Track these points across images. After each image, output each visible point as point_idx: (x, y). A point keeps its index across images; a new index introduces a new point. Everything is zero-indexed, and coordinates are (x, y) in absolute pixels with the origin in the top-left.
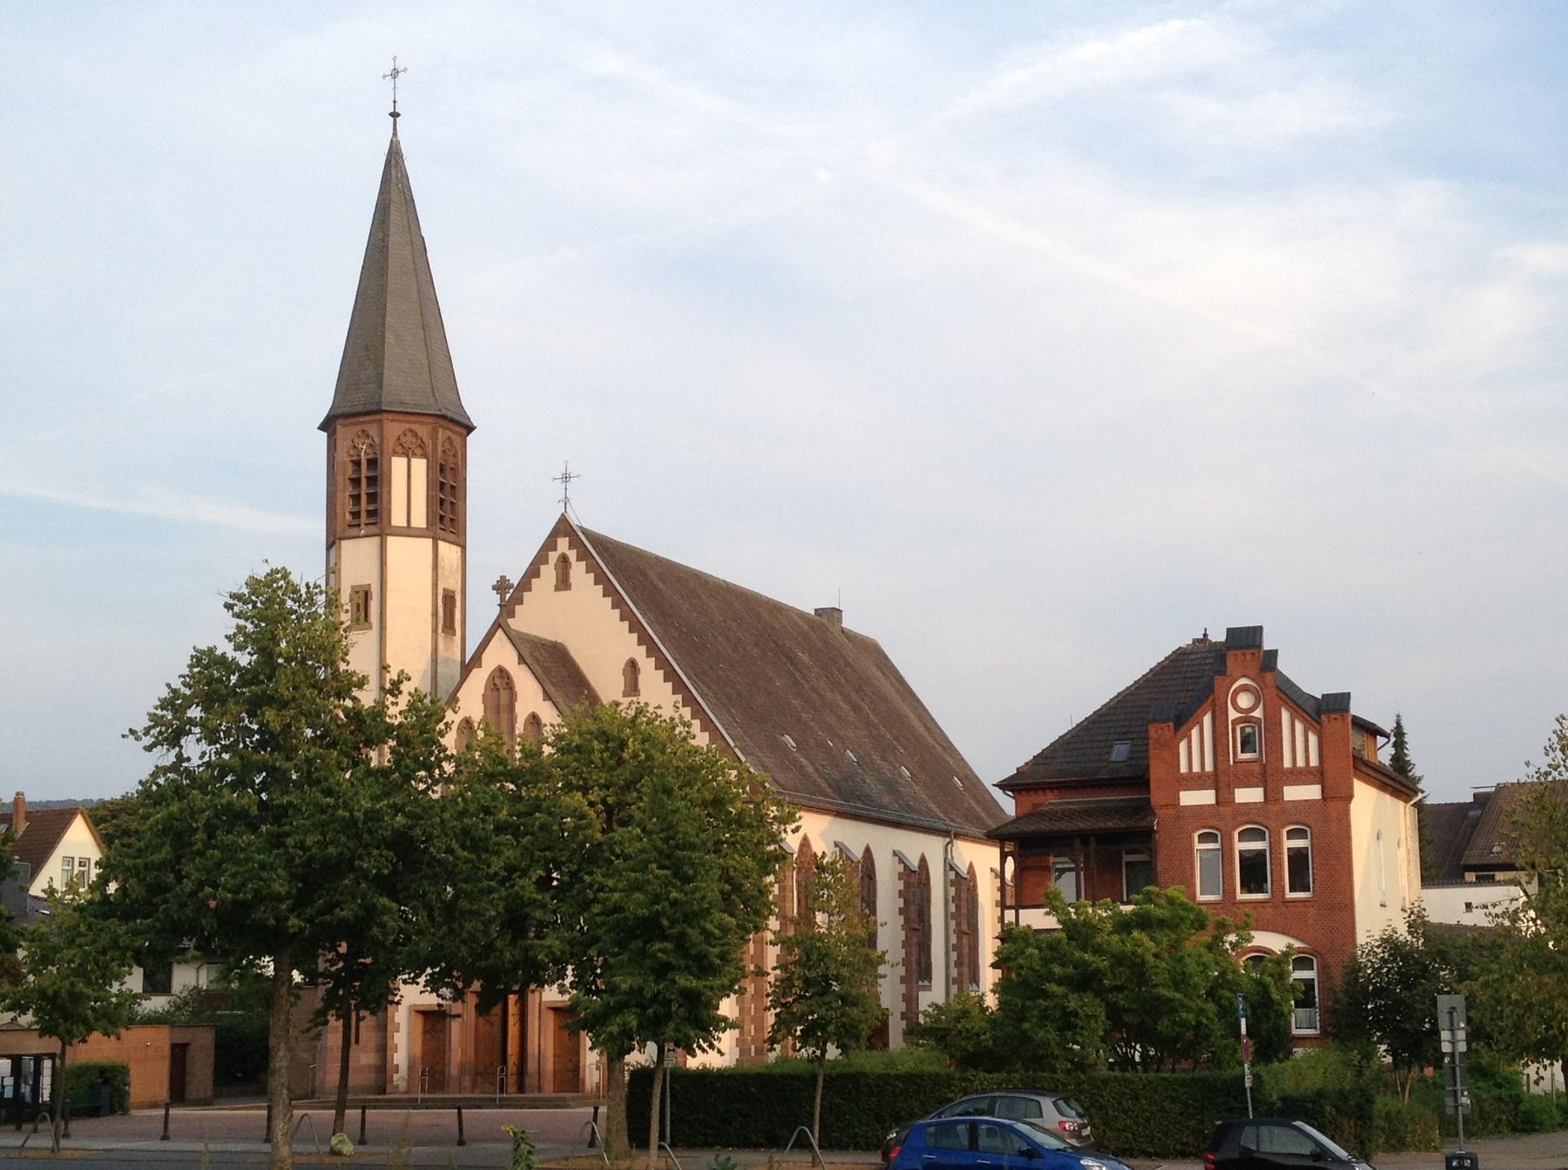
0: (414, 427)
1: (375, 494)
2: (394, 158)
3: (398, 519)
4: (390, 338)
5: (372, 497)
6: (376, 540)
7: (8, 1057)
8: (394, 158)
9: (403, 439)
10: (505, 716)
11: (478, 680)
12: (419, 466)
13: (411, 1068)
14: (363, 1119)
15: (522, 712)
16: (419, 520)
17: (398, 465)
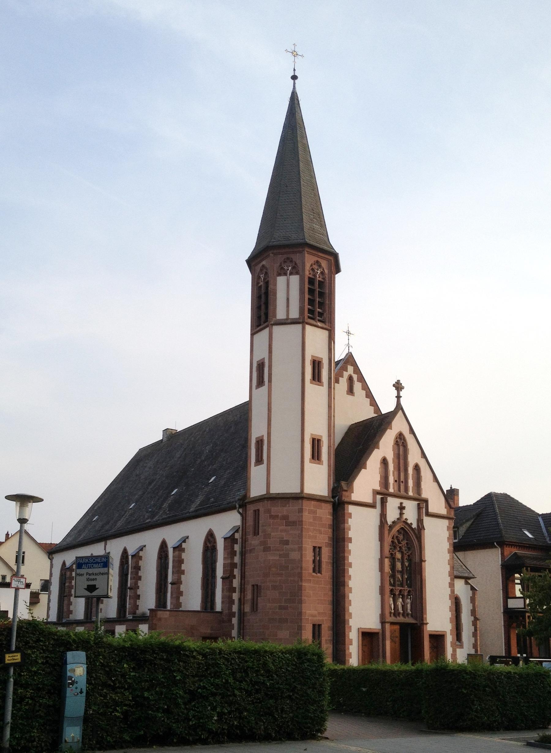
2: (294, 100)
3: (281, 314)
8: (294, 100)
12: (295, 280)
16: (294, 314)
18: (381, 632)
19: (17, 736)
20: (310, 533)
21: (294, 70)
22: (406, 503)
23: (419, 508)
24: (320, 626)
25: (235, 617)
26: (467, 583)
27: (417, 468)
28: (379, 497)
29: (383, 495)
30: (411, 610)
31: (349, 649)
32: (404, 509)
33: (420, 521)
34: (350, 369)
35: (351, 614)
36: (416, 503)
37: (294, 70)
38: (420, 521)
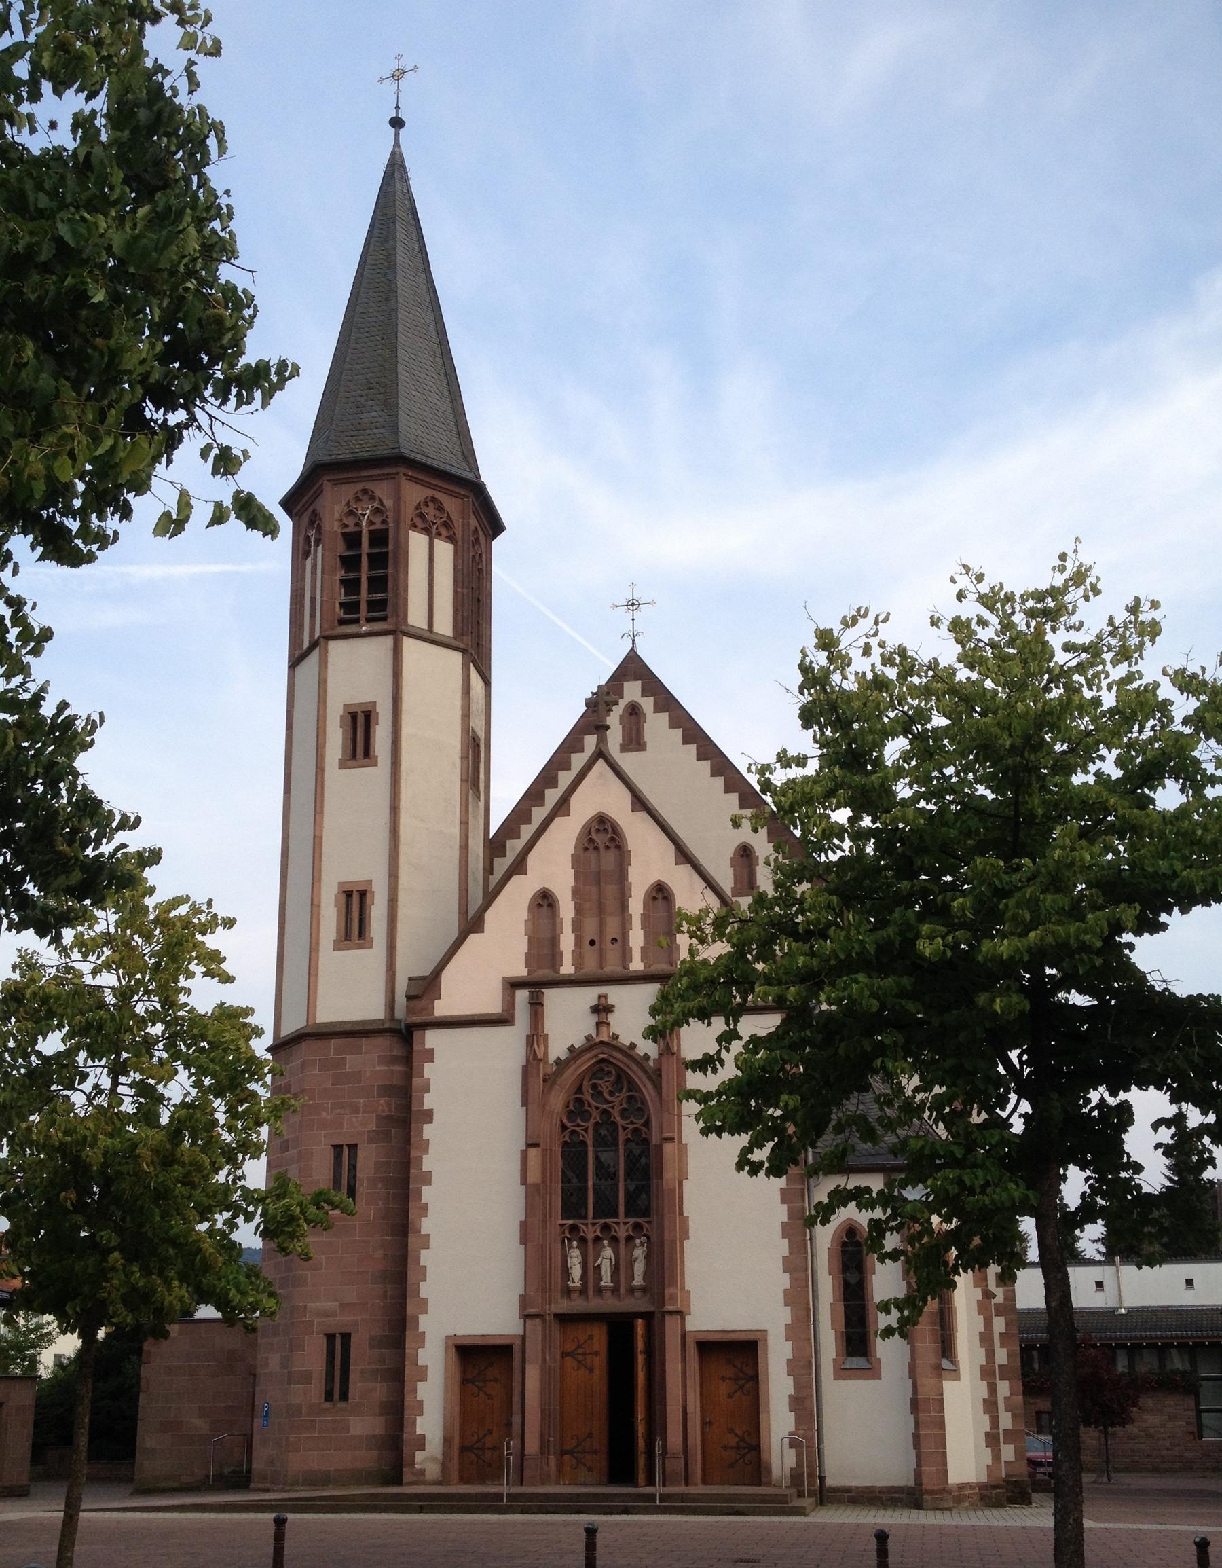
0: (439, 495)
1: (384, 578)
2: (396, 170)
3: (416, 617)
4: (403, 375)
5: (378, 583)
6: (388, 640)
7: (514, 994)
8: (396, 170)
9: (424, 510)
10: (610, 890)
11: (563, 838)
13: (447, 1441)
14: (279, 1536)
15: (640, 880)
17: (417, 542)
18: (518, 1342)
20: (324, 1114)
21: (397, 107)
22: (616, 995)
24: (346, 1337)
25: (1001, 1334)
28: (522, 996)
29: (535, 984)
30: (646, 1276)
31: (415, 1391)
34: (632, 690)
35: (425, 1301)
37: (397, 107)
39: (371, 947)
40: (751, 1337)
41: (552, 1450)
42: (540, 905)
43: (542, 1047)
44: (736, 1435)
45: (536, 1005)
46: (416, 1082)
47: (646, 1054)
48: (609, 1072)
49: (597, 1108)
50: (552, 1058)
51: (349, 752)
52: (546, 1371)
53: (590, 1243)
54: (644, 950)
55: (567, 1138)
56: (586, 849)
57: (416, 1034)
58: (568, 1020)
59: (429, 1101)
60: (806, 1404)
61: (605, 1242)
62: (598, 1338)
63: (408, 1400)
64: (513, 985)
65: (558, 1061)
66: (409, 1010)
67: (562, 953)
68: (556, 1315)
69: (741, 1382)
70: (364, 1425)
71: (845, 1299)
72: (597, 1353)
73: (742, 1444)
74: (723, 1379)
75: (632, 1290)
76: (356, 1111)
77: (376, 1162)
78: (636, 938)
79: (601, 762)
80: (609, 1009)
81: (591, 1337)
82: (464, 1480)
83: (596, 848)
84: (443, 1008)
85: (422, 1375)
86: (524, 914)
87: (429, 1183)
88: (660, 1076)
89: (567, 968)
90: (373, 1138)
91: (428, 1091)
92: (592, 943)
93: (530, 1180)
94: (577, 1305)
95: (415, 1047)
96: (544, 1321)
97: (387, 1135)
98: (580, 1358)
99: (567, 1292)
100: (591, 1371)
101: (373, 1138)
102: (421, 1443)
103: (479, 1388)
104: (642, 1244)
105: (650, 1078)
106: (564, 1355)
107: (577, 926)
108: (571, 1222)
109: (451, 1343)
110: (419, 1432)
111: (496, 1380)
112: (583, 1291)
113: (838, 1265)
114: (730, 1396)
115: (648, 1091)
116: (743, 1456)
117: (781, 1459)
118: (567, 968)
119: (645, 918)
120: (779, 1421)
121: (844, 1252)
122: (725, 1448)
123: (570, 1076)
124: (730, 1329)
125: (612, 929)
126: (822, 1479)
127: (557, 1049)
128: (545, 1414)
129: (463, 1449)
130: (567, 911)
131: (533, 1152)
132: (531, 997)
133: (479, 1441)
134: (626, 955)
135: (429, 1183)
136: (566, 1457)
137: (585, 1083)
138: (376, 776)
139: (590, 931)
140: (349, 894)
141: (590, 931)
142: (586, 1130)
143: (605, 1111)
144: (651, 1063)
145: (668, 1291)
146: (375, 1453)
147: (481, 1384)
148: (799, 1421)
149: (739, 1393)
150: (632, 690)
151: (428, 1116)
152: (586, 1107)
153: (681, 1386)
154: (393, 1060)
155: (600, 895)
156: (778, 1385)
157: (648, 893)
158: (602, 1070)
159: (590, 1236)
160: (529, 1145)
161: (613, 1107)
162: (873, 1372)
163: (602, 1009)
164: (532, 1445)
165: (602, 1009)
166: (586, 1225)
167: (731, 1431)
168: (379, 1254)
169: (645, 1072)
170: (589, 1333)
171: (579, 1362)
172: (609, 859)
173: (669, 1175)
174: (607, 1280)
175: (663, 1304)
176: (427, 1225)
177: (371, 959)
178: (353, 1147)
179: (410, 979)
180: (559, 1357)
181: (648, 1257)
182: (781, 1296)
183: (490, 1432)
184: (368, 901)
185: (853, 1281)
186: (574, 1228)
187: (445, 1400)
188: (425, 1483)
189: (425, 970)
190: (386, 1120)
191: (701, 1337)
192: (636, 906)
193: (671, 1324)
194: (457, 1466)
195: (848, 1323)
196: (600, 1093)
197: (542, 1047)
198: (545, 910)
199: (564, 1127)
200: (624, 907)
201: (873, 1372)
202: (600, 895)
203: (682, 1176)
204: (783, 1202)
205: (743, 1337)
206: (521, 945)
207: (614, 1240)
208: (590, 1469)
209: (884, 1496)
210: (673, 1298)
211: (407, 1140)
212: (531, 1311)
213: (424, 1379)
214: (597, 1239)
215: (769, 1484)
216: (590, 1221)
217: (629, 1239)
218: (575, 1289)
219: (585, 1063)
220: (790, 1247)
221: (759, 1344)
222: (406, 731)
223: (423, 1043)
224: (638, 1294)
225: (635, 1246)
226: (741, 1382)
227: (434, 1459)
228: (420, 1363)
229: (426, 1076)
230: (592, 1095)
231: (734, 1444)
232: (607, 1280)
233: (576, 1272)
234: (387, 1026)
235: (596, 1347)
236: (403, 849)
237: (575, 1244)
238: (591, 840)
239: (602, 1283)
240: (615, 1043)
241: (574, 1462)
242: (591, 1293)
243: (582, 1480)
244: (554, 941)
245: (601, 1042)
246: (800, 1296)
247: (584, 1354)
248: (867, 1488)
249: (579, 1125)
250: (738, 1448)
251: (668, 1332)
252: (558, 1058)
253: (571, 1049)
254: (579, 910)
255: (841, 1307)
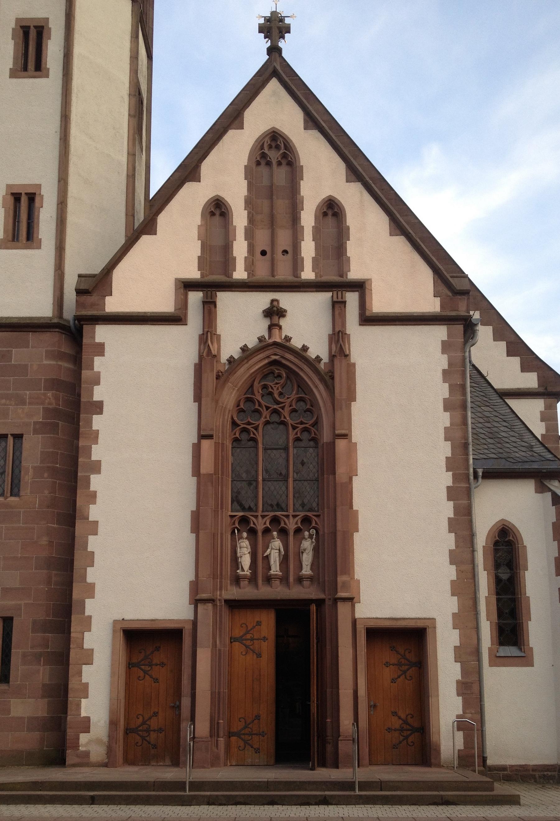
10: (282, 205)
13: (113, 724)
18: (188, 628)
19: (250, 760)
22: (286, 300)
23: (338, 306)
26: (541, 488)
27: (331, 209)
28: (195, 298)
29: (210, 285)
31: (80, 673)
32: (284, 316)
33: (338, 339)
35: (92, 587)
36: (325, 297)
38: (338, 339)
39: (39, 247)
40: (420, 624)
41: (221, 734)
42: (212, 214)
43: (216, 345)
44: (400, 718)
45: (209, 305)
46: (85, 374)
47: (318, 357)
48: (279, 376)
49: (268, 408)
50: (224, 357)
51: (21, 62)
52: (216, 656)
53: (260, 534)
54: (315, 261)
55: (237, 435)
56: (258, 163)
57: (86, 328)
58: (240, 322)
59: (97, 453)
60: (471, 690)
61: (275, 533)
62: (267, 623)
63: (73, 684)
64: (187, 286)
65: (231, 360)
66: (79, 304)
67: (235, 259)
68: (226, 601)
69: (404, 668)
70: (26, 706)
71: (498, 594)
72: (265, 639)
73: (405, 727)
74: (387, 664)
75: (300, 580)
76: (22, 402)
77: (42, 453)
78: (308, 249)
79: (274, 84)
80: (281, 313)
81: (259, 623)
82: (129, 761)
83: (269, 164)
84: (113, 304)
85: (88, 657)
86: (197, 220)
87: (101, 412)
88: (332, 378)
89: (240, 273)
90: (39, 429)
91: (98, 383)
92: (264, 253)
93: (203, 471)
94: (246, 592)
95: (85, 341)
96: (215, 606)
97: (54, 428)
98: (248, 643)
99: (237, 580)
100: (259, 656)
101: (39, 429)
102: (85, 725)
103: (145, 672)
104: (311, 536)
105: (322, 379)
106: (233, 640)
107: (249, 235)
108: (241, 514)
109: (119, 627)
110: (83, 714)
111: (162, 664)
112: (253, 579)
113: (491, 563)
114: (393, 681)
115: (320, 393)
116: (406, 738)
117: (448, 740)
118: (240, 273)
119: (317, 231)
120: (447, 706)
121: (496, 551)
122: (389, 730)
123: (243, 374)
124: (406, 617)
125: (283, 239)
126: (484, 759)
127: (229, 348)
128: (216, 698)
129: (128, 731)
130: (240, 219)
131: (206, 444)
132: (205, 296)
133: (144, 723)
134: (297, 264)
135: (101, 412)
136: (233, 739)
137: (256, 383)
138: (48, 86)
139: (262, 242)
140: (17, 197)
141: (262, 242)
142: (256, 428)
143: (275, 411)
144: (322, 366)
145: (341, 579)
146: (37, 735)
147: (147, 668)
148: (466, 705)
149: (402, 678)
150: (274, 111)
151: (96, 467)
152: (270, 390)
153: (351, 671)
154: (61, 356)
155: (272, 207)
156: (446, 671)
157: (319, 208)
158: (273, 373)
159: (260, 527)
160: (202, 437)
161: (283, 408)
162: (525, 659)
163: (274, 313)
164: (202, 727)
165: (274, 313)
166: (256, 517)
167: (395, 714)
168: (44, 541)
169: (316, 371)
170: (257, 619)
171: (247, 647)
172: (281, 175)
173: (341, 470)
174: (275, 569)
175: (336, 592)
176: (95, 512)
177: (42, 258)
178: (18, 437)
179: (80, 276)
180: (227, 641)
181: (316, 550)
182: (448, 587)
183: (156, 714)
184: (37, 204)
185: (504, 577)
186: (244, 520)
187: (112, 683)
188: (88, 764)
189: (96, 268)
190: (53, 413)
191: (372, 624)
192: (308, 219)
193: (343, 609)
194: (121, 748)
195: (500, 614)
196: (271, 394)
197: (216, 345)
198: (217, 218)
199: (234, 424)
200: (295, 219)
201: (525, 659)
202: (272, 207)
203: (352, 472)
204: (449, 499)
205: (412, 624)
206: (194, 249)
207: (283, 532)
208: (257, 751)
209: (537, 774)
210: (346, 585)
211: (76, 434)
212: (204, 596)
213: (90, 662)
214: (267, 531)
215: (439, 765)
216: (260, 513)
217: (298, 531)
218: (245, 577)
219: (257, 363)
220: (456, 541)
221: (429, 631)
222: (78, 50)
223: (93, 337)
224: (306, 583)
225: (304, 538)
226: (404, 668)
227: (98, 741)
228: (86, 646)
229: (96, 369)
230: (263, 396)
231: (397, 726)
232: (275, 569)
233: (246, 561)
234: (55, 321)
235: (264, 633)
236: (73, 159)
237: (245, 535)
238: (264, 155)
239: (272, 572)
240: (288, 344)
241: (242, 744)
242: (260, 581)
243: (249, 761)
244: (227, 248)
245: (275, 344)
246: (464, 587)
247: (252, 639)
248: (521, 766)
249: (249, 423)
250: (401, 730)
251: (340, 617)
252: (231, 357)
253: (244, 349)
254: (251, 220)
255: (494, 599)
